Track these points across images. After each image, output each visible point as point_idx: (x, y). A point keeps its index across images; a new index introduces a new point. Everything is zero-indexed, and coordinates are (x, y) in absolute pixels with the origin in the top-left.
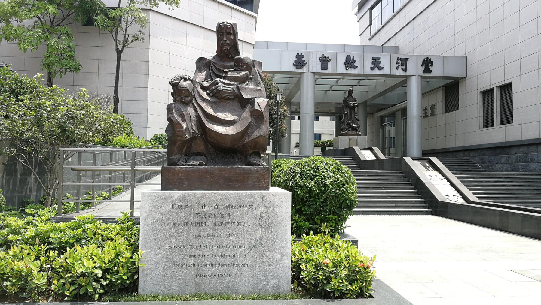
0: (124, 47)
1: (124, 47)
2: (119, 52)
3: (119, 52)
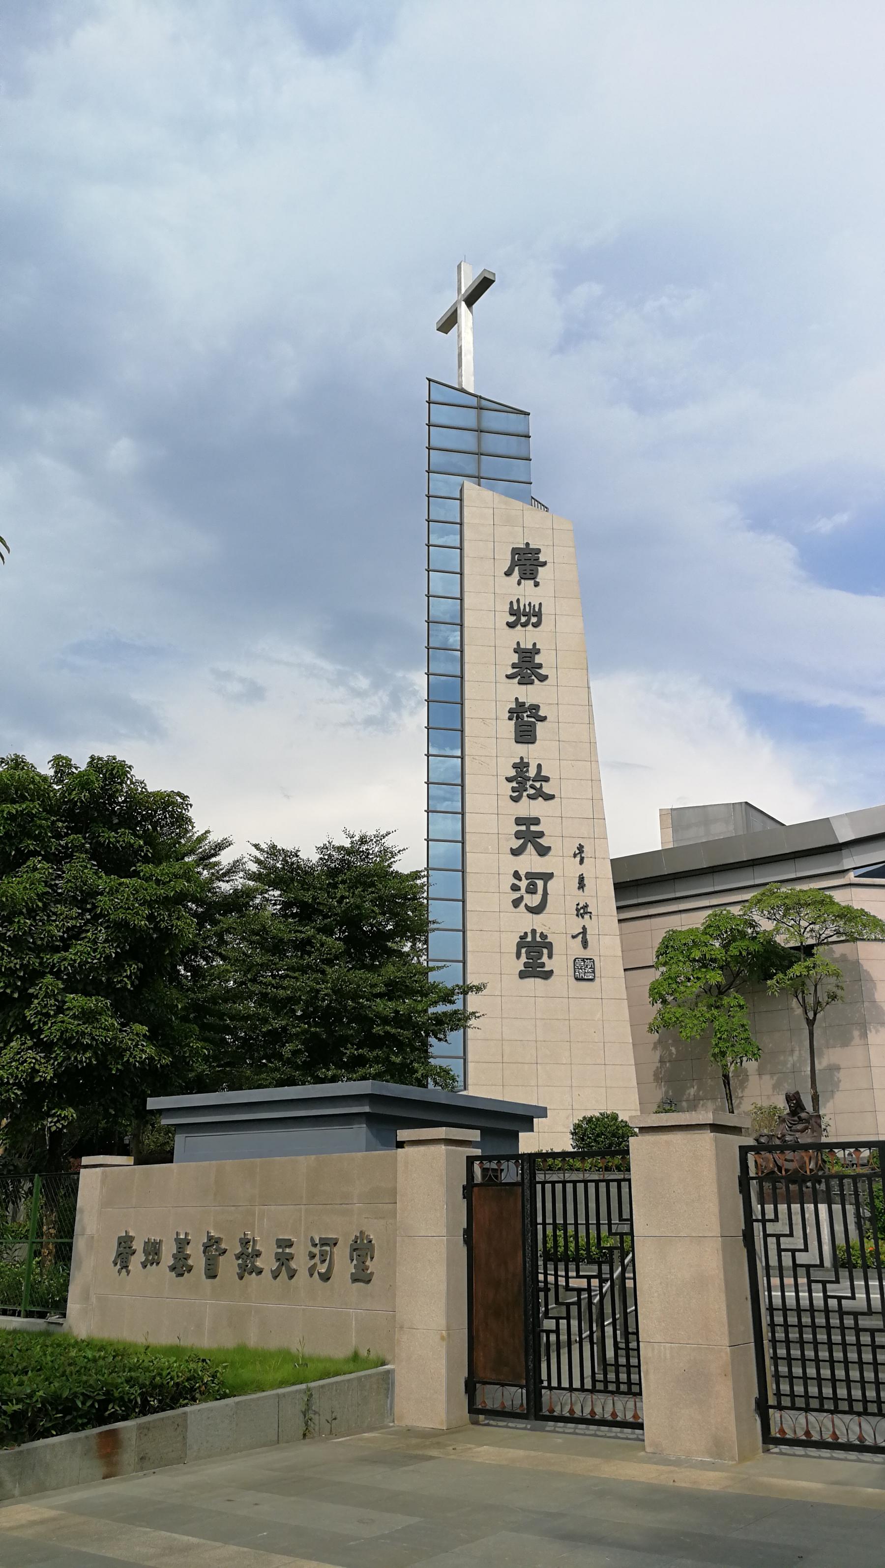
0: (815, 1014)
1: (815, 1014)
2: (811, 1023)
3: (811, 1023)
